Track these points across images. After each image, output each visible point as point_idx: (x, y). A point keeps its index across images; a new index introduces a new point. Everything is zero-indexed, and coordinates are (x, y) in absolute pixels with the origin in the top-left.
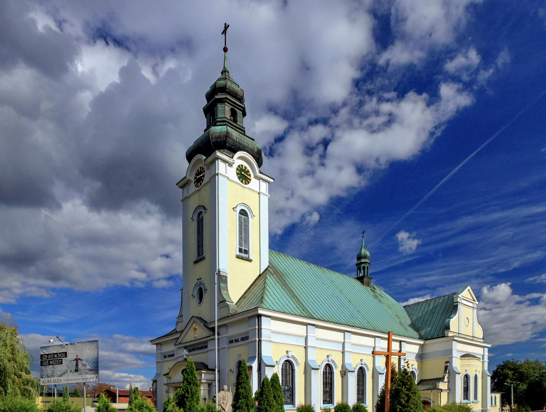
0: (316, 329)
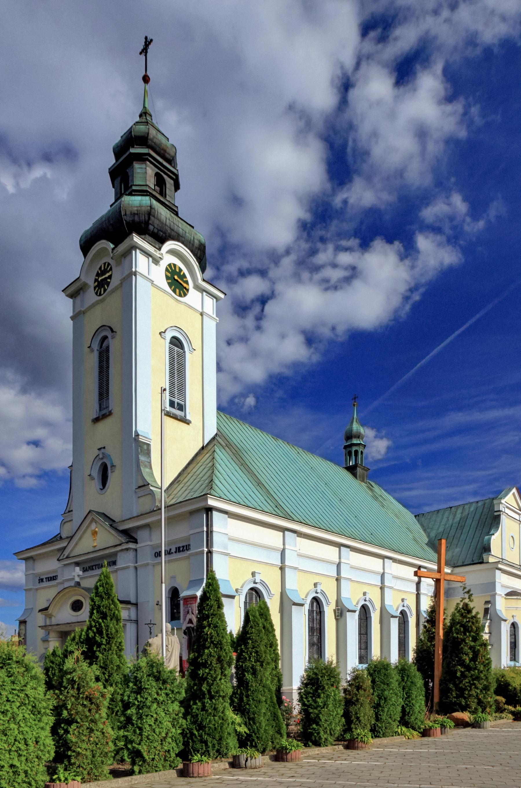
0: (299, 539)
